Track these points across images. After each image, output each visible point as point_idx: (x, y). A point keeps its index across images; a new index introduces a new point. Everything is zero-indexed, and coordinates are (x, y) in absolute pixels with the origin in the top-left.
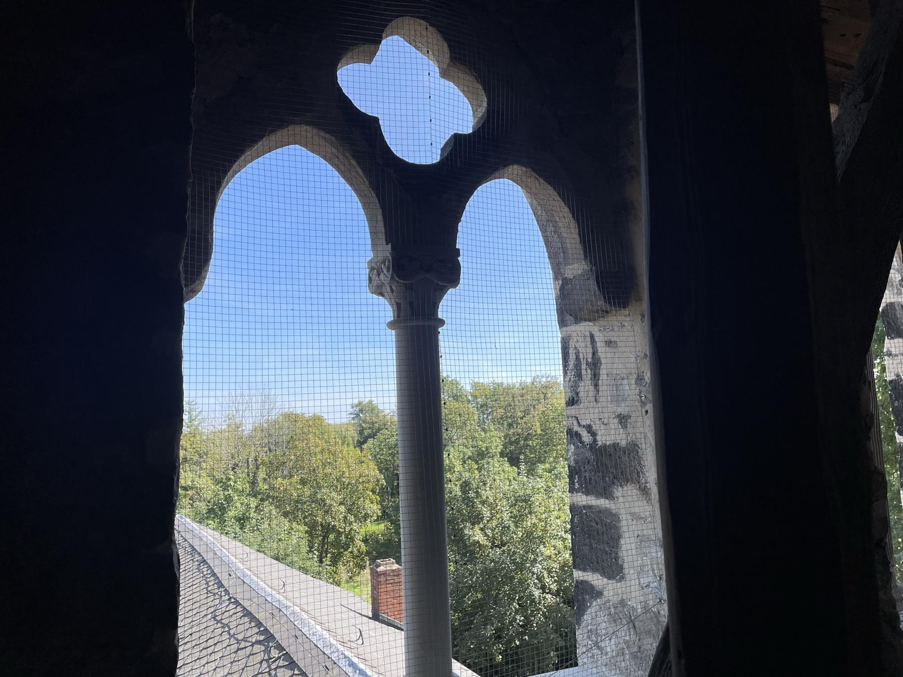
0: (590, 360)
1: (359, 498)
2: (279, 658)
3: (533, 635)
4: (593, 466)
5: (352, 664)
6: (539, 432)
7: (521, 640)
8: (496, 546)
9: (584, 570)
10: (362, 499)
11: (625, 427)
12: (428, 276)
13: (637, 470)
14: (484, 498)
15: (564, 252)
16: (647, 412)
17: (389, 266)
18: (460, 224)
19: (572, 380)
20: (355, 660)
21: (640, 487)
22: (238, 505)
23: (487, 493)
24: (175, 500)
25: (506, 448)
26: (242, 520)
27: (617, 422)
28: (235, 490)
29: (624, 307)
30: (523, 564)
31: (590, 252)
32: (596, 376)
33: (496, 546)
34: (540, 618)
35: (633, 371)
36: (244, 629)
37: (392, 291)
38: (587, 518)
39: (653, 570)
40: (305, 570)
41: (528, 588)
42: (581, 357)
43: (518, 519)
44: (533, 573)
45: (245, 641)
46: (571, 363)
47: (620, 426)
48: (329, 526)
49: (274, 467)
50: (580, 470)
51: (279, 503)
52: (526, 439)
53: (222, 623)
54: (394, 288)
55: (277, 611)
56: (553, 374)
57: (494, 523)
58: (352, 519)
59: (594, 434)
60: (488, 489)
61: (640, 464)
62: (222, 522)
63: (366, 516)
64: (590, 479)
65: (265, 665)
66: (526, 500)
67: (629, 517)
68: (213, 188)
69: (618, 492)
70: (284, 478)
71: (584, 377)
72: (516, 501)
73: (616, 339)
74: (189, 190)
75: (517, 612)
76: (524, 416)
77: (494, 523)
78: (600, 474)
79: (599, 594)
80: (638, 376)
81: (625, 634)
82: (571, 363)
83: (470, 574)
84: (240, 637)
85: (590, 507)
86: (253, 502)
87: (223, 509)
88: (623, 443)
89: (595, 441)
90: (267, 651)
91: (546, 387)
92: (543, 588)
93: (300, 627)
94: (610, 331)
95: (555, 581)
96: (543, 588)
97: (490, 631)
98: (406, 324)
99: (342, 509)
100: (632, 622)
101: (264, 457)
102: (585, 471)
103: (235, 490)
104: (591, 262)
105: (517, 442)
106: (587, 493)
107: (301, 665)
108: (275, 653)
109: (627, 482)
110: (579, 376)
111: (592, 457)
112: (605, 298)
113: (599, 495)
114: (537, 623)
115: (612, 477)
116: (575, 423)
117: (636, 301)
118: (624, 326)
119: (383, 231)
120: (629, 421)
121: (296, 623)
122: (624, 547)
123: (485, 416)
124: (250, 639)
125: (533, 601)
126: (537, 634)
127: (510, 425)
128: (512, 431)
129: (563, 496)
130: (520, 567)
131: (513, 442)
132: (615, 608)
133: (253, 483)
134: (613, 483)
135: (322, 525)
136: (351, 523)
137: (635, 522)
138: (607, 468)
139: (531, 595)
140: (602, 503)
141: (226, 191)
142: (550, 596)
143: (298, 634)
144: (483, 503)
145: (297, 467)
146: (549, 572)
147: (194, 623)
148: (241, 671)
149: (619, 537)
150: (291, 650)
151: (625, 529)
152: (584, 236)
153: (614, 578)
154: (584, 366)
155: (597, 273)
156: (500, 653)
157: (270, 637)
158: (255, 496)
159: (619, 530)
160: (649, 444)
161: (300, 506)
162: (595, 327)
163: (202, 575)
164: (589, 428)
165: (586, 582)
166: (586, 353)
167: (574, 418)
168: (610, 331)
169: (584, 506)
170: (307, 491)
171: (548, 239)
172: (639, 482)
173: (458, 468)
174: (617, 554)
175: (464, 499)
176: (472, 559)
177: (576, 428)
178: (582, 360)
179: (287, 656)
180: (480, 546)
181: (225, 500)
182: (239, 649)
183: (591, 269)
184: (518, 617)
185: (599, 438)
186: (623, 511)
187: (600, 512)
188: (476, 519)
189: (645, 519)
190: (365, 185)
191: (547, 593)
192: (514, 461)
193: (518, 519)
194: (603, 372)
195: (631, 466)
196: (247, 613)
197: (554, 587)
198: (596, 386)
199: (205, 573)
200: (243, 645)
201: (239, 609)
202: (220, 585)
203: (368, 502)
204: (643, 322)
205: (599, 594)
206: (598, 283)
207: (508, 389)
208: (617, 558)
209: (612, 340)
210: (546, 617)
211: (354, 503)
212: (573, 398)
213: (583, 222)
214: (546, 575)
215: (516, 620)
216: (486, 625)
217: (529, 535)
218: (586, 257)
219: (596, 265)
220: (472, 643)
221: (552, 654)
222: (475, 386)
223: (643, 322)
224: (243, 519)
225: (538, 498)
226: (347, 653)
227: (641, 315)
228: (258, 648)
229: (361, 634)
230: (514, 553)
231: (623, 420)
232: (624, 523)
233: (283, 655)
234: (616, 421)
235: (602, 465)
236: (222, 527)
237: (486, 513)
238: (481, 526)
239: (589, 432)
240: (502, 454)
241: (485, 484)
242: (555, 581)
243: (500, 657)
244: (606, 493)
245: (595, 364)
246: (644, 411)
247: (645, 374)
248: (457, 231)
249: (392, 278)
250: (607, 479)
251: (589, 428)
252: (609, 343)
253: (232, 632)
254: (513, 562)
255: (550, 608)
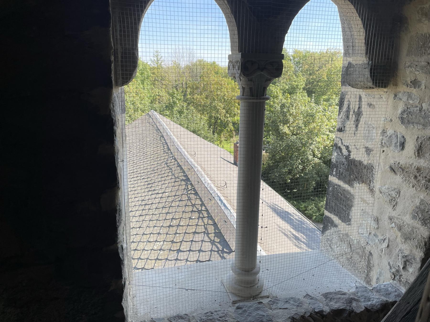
0: (356, 110)
1: (232, 106)
2: (191, 189)
3: (306, 174)
4: (346, 167)
5: (220, 200)
6: (326, 79)
7: (300, 176)
8: (294, 135)
9: (331, 213)
10: (233, 107)
11: (368, 154)
12: (262, 73)
13: (370, 179)
14: (291, 112)
15: (353, 47)
16: (384, 151)
17: (239, 66)
18: (286, 35)
19: (343, 117)
20: (222, 198)
21: (369, 188)
22: (178, 105)
23: (293, 111)
24: (118, 225)
25: (306, 85)
26: (181, 112)
27: (364, 150)
28: (177, 99)
29: (385, 87)
30: (305, 144)
31: (370, 52)
32: (357, 121)
33: (294, 135)
34: (310, 168)
35: (381, 126)
36: (177, 172)
37: (241, 80)
38: (336, 190)
39: (367, 228)
40: (205, 138)
41: (306, 155)
42: (351, 107)
43: (306, 124)
44: (310, 149)
45: (178, 178)
46: (345, 109)
47: (366, 153)
48: (218, 118)
49: (195, 88)
50: (338, 167)
51: (197, 106)
52: (318, 82)
53: (169, 167)
54: (241, 78)
55: (191, 168)
56: (338, 47)
57: (295, 125)
58: (228, 116)
59: (349, 152)
60: (294, 108)
61: (372, 177)
62: (172, 113)
63: (235, 115)
64: (342, 173)
65: (185, 191)
66: (312, 116)
67: (360, 200)
68: (135, 24)
69: (356, 185)
70: (198, 95)
71: (350, 119)
72: (307, 115)
73: (374, 103)
74: (112, 58)
75: (300, 164)
76: (319, 70)
77: (295, 125)
78: (349, 173)
79: (336, 226)
80: (384, 130)
81: (345, 247)
82: (345, 109)
83: (280, 146)
84: (176, 175)
85: (339, 186)
86: (185, 105)
87: (172, 107)
88: (365, 163)
89: (349, 155)
90: (186, 185)
91: (332, 54)
92: (314, 156)
93: (200, 177)
94: (372, 98)
95: (320, 153)
96: (314, 156)
97: (286, 170)
98: (246, 101)
99: (224, 111)
100: (350, 246)
101: (190, 83)
102: (341, 168)
103: (177, 99)
104: (369, 58)
105: (313, 83)
106: (339, 179)
107: (200, 195)
108: (190, 187)
109: (363, 183)
110: (348, 117)
111: (346, 163)
112: (373, 82)
113: (345, 182)
114: (308, 170)
115: (355, 176)
116: (340, 142)
117: (394, 85)
118: (382, 98)
119: (237, 41)
120: (371, 152)
121: (199, 175)
122: (353, 212)
123: (298, 68)
124: (180, 178)
125: (308, 160)
126: (308, 174)
127: (310, 74)
128: (311, 77)
129: (331, 114)
130: (304, 145)
131: (310, 83)
132: (343, 236)
133: (185, 95)
134: (355, 180)
135: (215, 117)
136: (227, 118)
137: (362, 202)
138: (353, 171)
139: (307, 158)
140: (346, 186)
141: (150, 8)
142: (316, 159)
143: (199, 180)
144: (291, 115)
145: (204, 89)
146: (318, 148)
147: (158, 164)
148: (176, 191)
149: (352, 206)
150: (196, 187)
151: (356, 203)
152: (368, 41)
153: (345, 223)
154: (351, 113)
155: (372, 66)
156: (290, 179)
157: (187, 179)
158: (185, 101)
159: (353, 203)
160: (380, 169)
161: (205, 108)
162: (363, 93)
163: (161, 142)
164: (347, 147)
165: (330, 218)
166: (354, 106)
167: (340, 139)
168: (372, 98)
169: (336, 184)
170: (209, 101)
171: (345, 29)
172: (369, 185)
173: (281, 97)
174: (349, 213)
175: (281, 112)
176: (282, 139)
177: (340, 145)
178: (351, 109)
179: (195, 190)
180: (286, 134)
181: (173, 103)
182: (175, 181)
183: (368, 63)
184: (300, 166)
185: (352, 154)
186: (357, 194)
187: (344, 190)
188: (286, 122)
189: (368, 204)
190: (229, 11)
191: (315, 158)
192: (310, 93)
193: (306, 124)
194: (362, 120)
195: (367, 175)
196: (179, 166)
197: (319, 156)
198: (357, 126)
199: (163, 142)
200: (177, 180)
201: (176, 163)
202: (169, 149)
203: (236, 109)
204: (395, 99)
205: (336, 226)
206: (371, 73)
207: (312, 55)
208: (348, 215)
209: (372, 103)
210: (313, 167)
211: (229, 109)
212: (342, 128)
213: (369, 30)
214: (316, 150)
215: (299, 167)
216: (284, 167)
217: (311, 131)
218: (366, 54)
219: (372, 60)
220: (277, 174)
221: (313, 183)
222: (296, 52)
223: (395, 99)
224: (181, 112)
225: (318, 116)
226: (219, 194)
227: (394, 94)
228: (183, 183)
229: (226, 184)
230: (302, 139)
231: (368, 151)
232: (356, 200)
233: (193, 188)
234: (364, 150)
235: (351, 168)
236: (171, 116)
237: (291, 120)
238: (288, 125)
239: (347, 149)
240: (304, 89)
241: (292, 106)
242: (320, 153)
243: (289, 180)
244: (350, 183)
245: (359, 114)
246: (382, 150)
247: (388, 130)
248: (284, 40)
249: (240, 75)
250: (352, 177)
251: (347, 147)
252: (370, 105)
253: (173, 172)
254: (302, 143)
255: (315, 164)
